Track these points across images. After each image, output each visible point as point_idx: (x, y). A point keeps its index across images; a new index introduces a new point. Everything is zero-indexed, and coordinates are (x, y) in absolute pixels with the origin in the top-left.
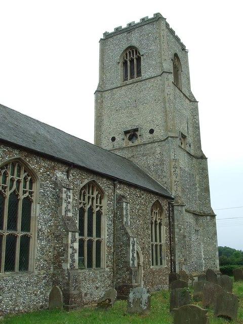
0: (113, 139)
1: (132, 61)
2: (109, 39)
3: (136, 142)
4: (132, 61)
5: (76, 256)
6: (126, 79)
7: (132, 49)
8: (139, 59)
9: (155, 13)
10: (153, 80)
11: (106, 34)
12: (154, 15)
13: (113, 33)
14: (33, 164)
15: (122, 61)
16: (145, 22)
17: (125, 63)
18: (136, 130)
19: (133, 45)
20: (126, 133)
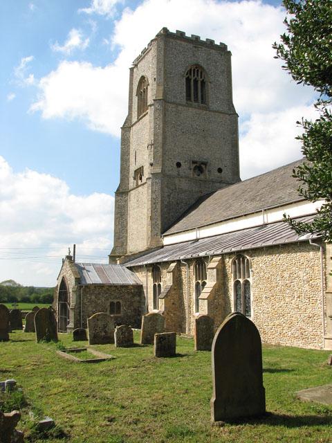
4: (196, 82)
11: (165, 30)
18: (205, 164)
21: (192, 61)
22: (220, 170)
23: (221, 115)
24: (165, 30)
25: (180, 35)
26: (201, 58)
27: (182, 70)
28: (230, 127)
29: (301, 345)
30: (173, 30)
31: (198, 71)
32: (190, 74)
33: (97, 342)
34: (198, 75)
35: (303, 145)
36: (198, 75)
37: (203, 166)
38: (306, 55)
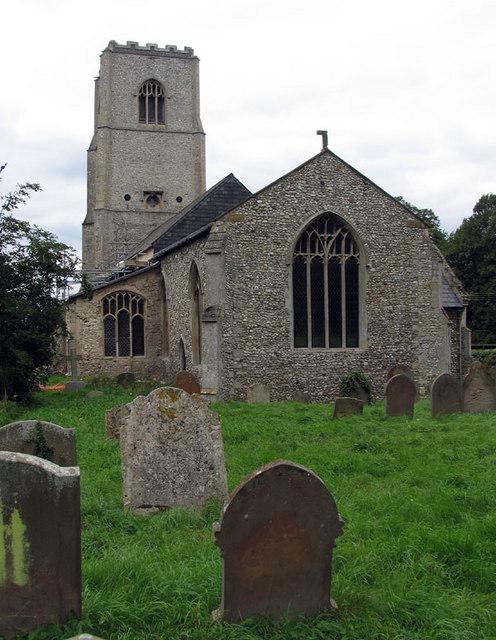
0: (127, 197)
1: (152, 99)
2: (121, 55)
3: (157, 208)
4: (152, 99)
5: (184, 239)
6: (142, 118)
7: (153, 84)
8: (161, 100)
9: (172, 44)
10: (183, 136)
11: (113, 43)
12: (186, 48)
13: (179, 52)
14: (27, 190)
15: (138, 94)
16: (171, 52)
17: (142, 99)
18: (161, 193)
19: (156, 78)
20: (146, 193)
25: (132, 48)
28: (416, 342)
30: (122, 42)
31: (154, 86)
37: (159, 196)
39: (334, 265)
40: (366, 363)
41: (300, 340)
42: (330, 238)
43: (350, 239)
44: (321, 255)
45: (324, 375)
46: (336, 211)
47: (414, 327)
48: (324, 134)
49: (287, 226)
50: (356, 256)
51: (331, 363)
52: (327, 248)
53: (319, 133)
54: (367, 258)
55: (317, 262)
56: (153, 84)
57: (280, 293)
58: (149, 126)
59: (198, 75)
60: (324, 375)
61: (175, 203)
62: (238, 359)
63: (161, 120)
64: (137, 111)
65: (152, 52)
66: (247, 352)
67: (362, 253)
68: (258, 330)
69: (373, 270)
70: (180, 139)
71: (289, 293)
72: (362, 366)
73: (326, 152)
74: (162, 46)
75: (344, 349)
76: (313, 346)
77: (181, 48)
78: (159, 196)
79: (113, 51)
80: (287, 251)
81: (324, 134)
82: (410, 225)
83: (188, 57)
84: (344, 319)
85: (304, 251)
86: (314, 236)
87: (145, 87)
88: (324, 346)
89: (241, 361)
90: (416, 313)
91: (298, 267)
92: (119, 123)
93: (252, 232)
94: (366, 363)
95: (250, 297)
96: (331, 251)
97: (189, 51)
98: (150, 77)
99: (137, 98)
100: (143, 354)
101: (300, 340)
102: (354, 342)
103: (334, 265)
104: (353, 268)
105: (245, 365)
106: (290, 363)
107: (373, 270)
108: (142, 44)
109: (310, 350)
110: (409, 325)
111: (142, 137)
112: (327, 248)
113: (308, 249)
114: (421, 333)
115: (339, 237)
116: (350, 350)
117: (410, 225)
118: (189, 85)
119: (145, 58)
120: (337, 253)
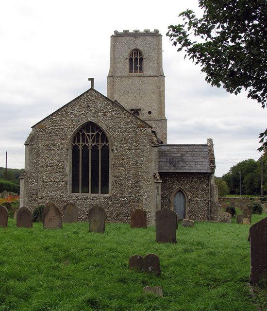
1: (136, 59)
2: (119, 38)
4: (136, 59)
7: (137, 51)
8: (141, 59)
9: (126, 29)
11: (116, 32)
13: (151, 33)
15: (128, 57)
16: (147, 33)
17: (131, 60)
18: (140, 110)
21: (133, 47)
22: (150, 113)
23: (152, 78)
24: (116, 32)
25: (126, 33)
26: (139, 44)
27: (126, 54)
28: (141, 192)
29: (95, 218)
30: (121, 31)
31: (137, 52)
32: (132, 56)
33: (47, 123)
34: (137, 55)
35: (233, 94)
36: (137, 55)
37: (139, 112)
38: (256, 22)
39: (95, 149)
40: (110, 203)
41: (75, 189)
42: (92, 135)
43: (104, 134)
44: (107, 144)
45: (86, 208)
46: (94, 120)
47: (141, 184)
48: (92, 80)
49: (67, 130)
50: (107, 144)
51: (90, 202)
52: (90, 141)
53: (90, 79)
54: (112, 147)
55: (85, 148)
56: (137, 51)
57: (63, 164)
58: (134, 74)
59: (161, 44)
60: (86, 208)
61: (148, 115)
62: (40, 198)
63: (141, 69)
64: (128, 66)
65: (136, 34)
66: (44, 194)
67: (110, 143)
68: (51, 183)
69: (116, 152)
70: (150, 80)
71: (111, 162)
72: (108, 204)
73: (92, 89)
74: (142, 30)
75: (100, 195)
76: (82, 192)
77: (152, 30)
78: (139, 112)
79: (117, 37)
80: (67, 142)
81: (92, 80)
82: (139, 126)
83: (117, 37)
84: (80, 177)
85: (78, 142)
86: (83, 134)
87: (132, 53)
88: (88, 192)
89: (42, 198)
90: (142, 176)
91: (75, 150)
92: (118, 74)
93: (50, 133)
94: (110, 203)
95: (47, 166)
96: (93, 142)
97: (157, 32)
98: (135, 48)
99: (128, 60)
100: (108, 193)
101: (75, 189)
102: (105, 190)
103: (95, 149)
104: (106, 151)
105: (44, 201)
106: (67, 201)
107: (116, 152)
108: (131, 31)
109: (80, 195)
110: (137, 182)
111: (130, 80)
112: (90, 141)
113: (81, 140)
114: (144, 187)
115: (98, 134)
116: (102, 195)
117: (139, 126)
118: (156, 50)
119: (132, 38)
120: (77, 143)
